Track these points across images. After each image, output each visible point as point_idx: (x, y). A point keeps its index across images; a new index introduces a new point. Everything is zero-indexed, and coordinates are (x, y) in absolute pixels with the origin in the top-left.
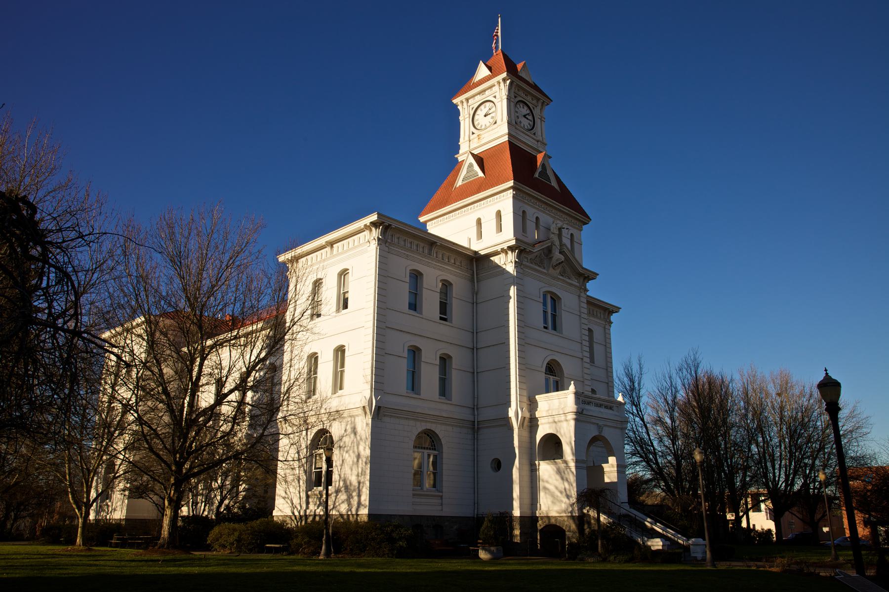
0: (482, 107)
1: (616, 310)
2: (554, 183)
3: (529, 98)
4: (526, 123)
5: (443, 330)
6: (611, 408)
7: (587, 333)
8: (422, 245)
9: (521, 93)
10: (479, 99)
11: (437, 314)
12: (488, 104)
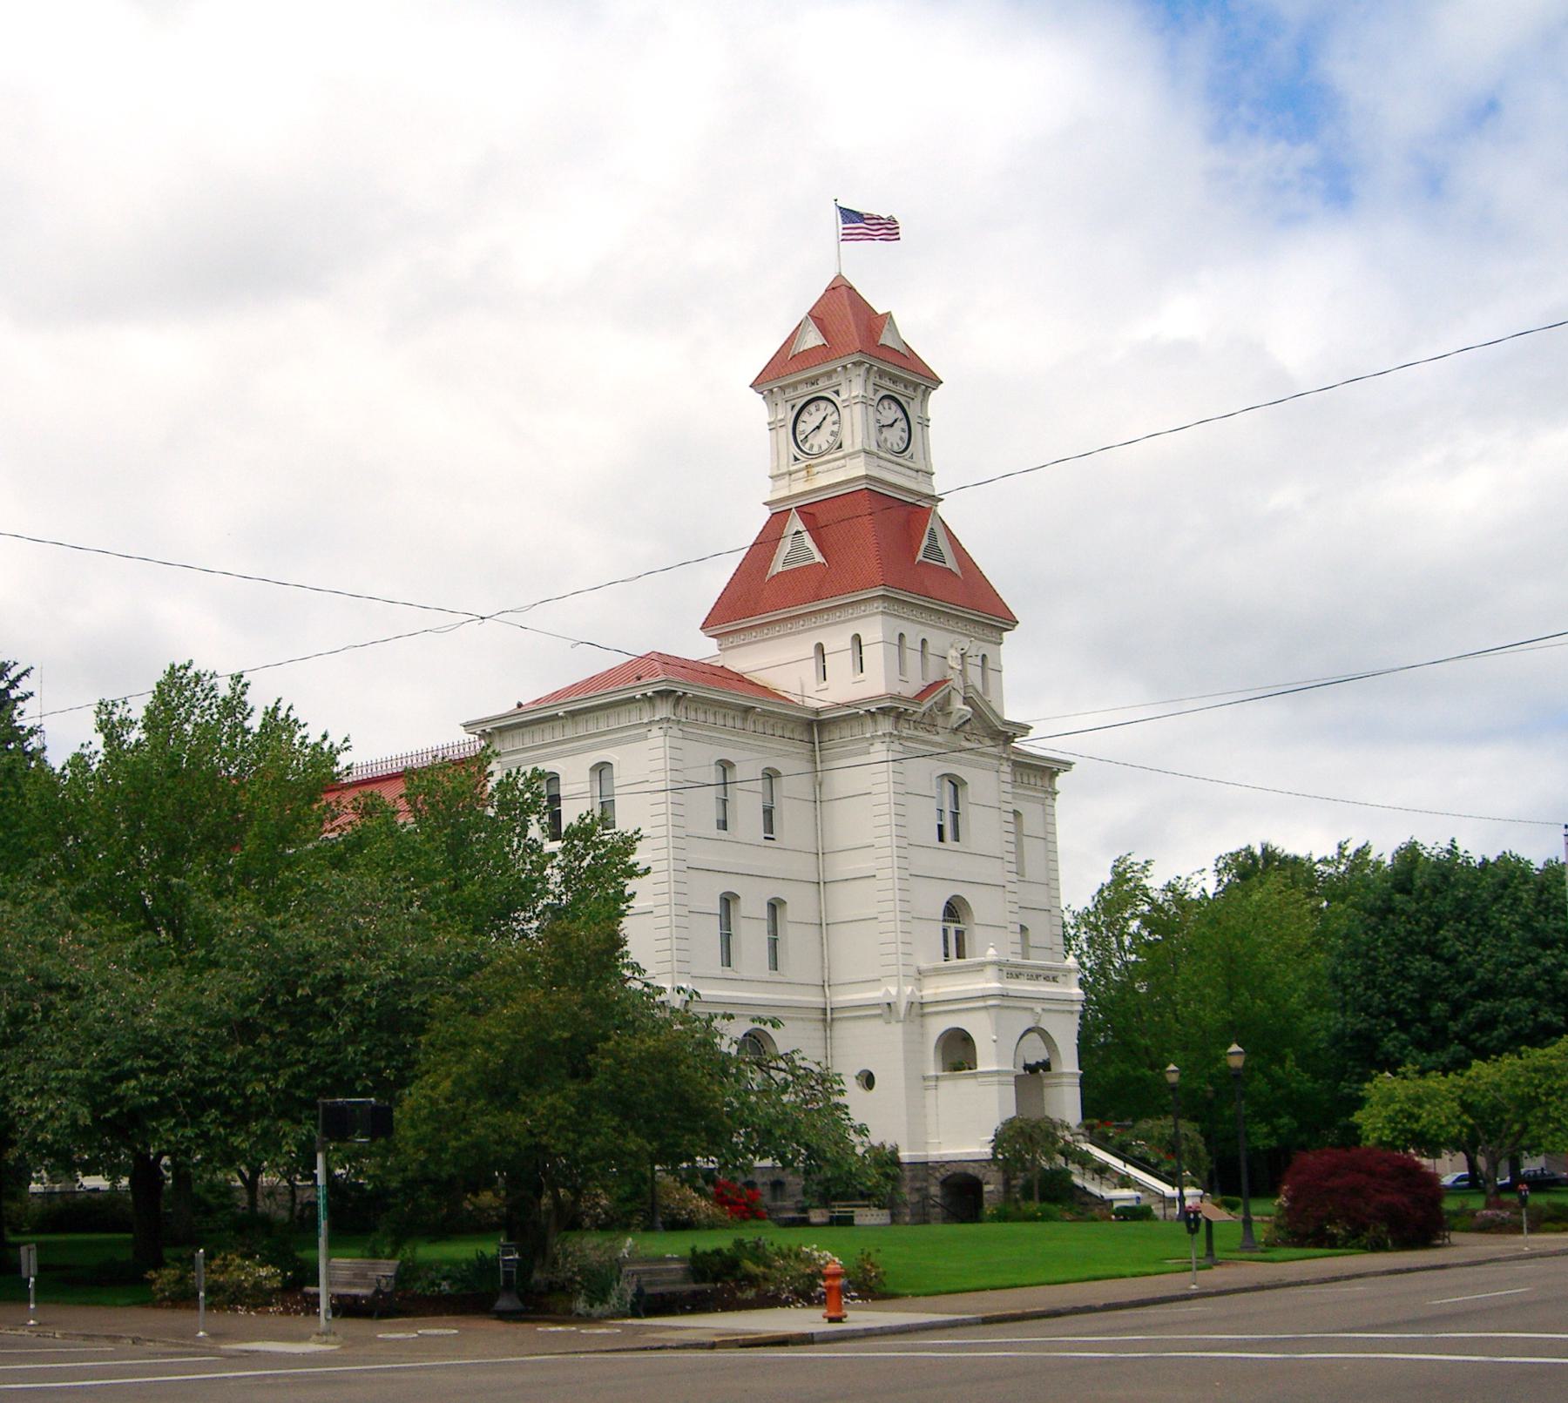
0: (812, 408)
1: (1068, 765)
2: (951, 563)
3: (900, 388)
4: (895, 436)
5: (768, 860)
6: (1054, 979)
7: (1011, 817)
8: (732, 713)
9: (886, 383)
10: (807, 392)
11: (760, 832)
12: (823, 404)
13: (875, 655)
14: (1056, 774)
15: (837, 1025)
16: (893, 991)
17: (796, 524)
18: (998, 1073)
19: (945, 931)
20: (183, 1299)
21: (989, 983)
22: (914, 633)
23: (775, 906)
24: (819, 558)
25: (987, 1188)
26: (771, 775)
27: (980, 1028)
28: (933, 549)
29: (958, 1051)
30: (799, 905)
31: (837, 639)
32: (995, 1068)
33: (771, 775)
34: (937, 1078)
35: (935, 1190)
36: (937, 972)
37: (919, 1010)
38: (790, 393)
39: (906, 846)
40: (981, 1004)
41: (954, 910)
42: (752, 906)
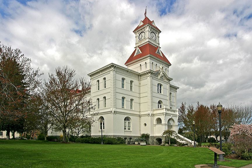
13: (148, 65)
14: (177, 89)
15: (141, 117)
16: (149, 112)
17: (138, 48)
18: (165, 124)
19: (158, 105)
20: (13, 144)
21: (164, 111)
22: (155, 63)
23: (132, 100)
24: (141, 52)
25: (162, 140)
26: (131, 82)
27: (162, 118)
28: (158, 52)
29: (159, 121)
30: (136, 100)
31: (143, 63)
32: (164, 123)
33: (131, 82)
34: (156, 125)
35: (155, 140)
36: (156, 110)
37: (153, 115)
38: (138, 32)
39: (152, 92)
40: (162, 114)
41: (160, 102)
42: (127, 99)
